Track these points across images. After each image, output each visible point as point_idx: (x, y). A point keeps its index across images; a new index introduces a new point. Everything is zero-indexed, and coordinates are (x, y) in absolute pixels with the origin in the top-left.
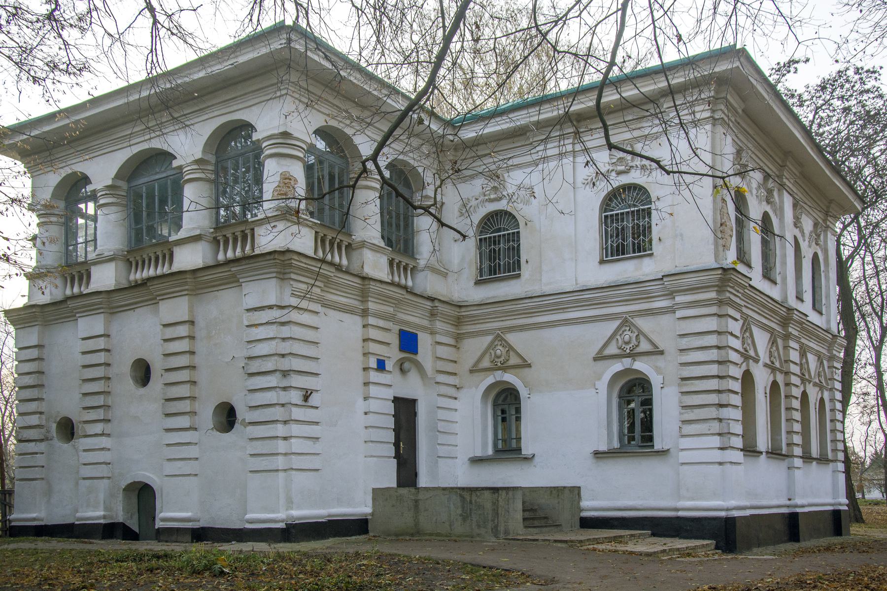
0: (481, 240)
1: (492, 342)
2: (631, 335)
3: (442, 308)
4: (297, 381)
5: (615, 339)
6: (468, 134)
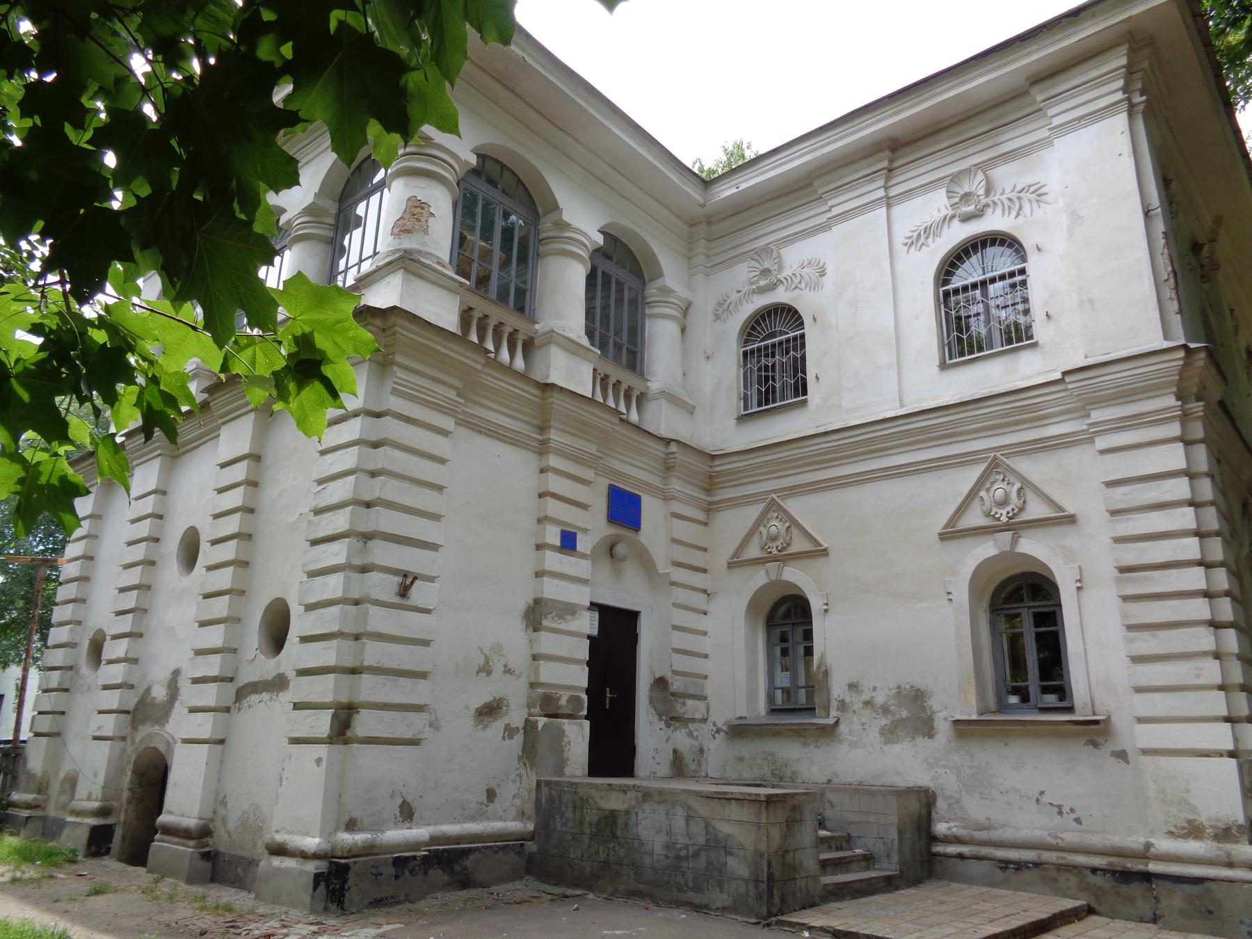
0: (745, 354)
3: (681, 456)
4: (383, 553)
5: (977, 499)
6: (726, 191)
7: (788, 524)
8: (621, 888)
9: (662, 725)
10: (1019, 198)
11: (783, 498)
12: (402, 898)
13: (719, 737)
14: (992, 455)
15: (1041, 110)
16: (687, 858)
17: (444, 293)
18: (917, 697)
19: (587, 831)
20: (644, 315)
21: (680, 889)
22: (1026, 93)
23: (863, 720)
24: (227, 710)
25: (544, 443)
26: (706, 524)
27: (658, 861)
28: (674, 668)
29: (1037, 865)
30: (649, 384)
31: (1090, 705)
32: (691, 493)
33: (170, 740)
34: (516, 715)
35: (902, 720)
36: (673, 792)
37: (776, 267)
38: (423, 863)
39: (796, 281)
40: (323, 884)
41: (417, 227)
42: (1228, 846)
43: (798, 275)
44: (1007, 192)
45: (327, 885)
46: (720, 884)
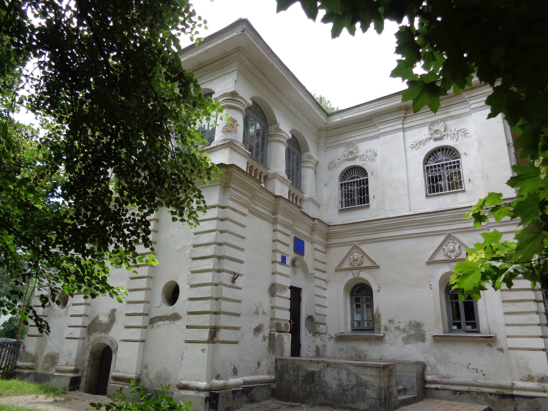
0: (341, 185)
1: (351, 250)
2: (455, 246)
3: (319, 226)
4: (228, 265)
7: (362, 255)
8: (317, 402)
9: (311, 335)
10: (457, 134)
12: (235, 407)
13: (332, 340)
14: (448, 232)
15: (466, 101)
16: (348, 390)
17: (242, 157)
18: (418, 326)
19: (301, 379)
20: (301, 166)
21: (345, 402)
23: (395, 335)
24: (146, 327)
25: (276, 219)
26: (325, 253)
27: (335, 391)
28: (316, 312)
29: (468, 392)
30: (304, 195)
31: (488, 331)
32: (323, 241)
33: (113, 340)
34: (266, 332)
35: (411, 335)
36: (340, 364)
37: (356, 151)
38: (242, 393)
39: (365, 157)
40: (208, 401)
41: (233, 130)
42: (543, 384)
44: (452, 131)
45: (210, 402)
46: (363, 401)
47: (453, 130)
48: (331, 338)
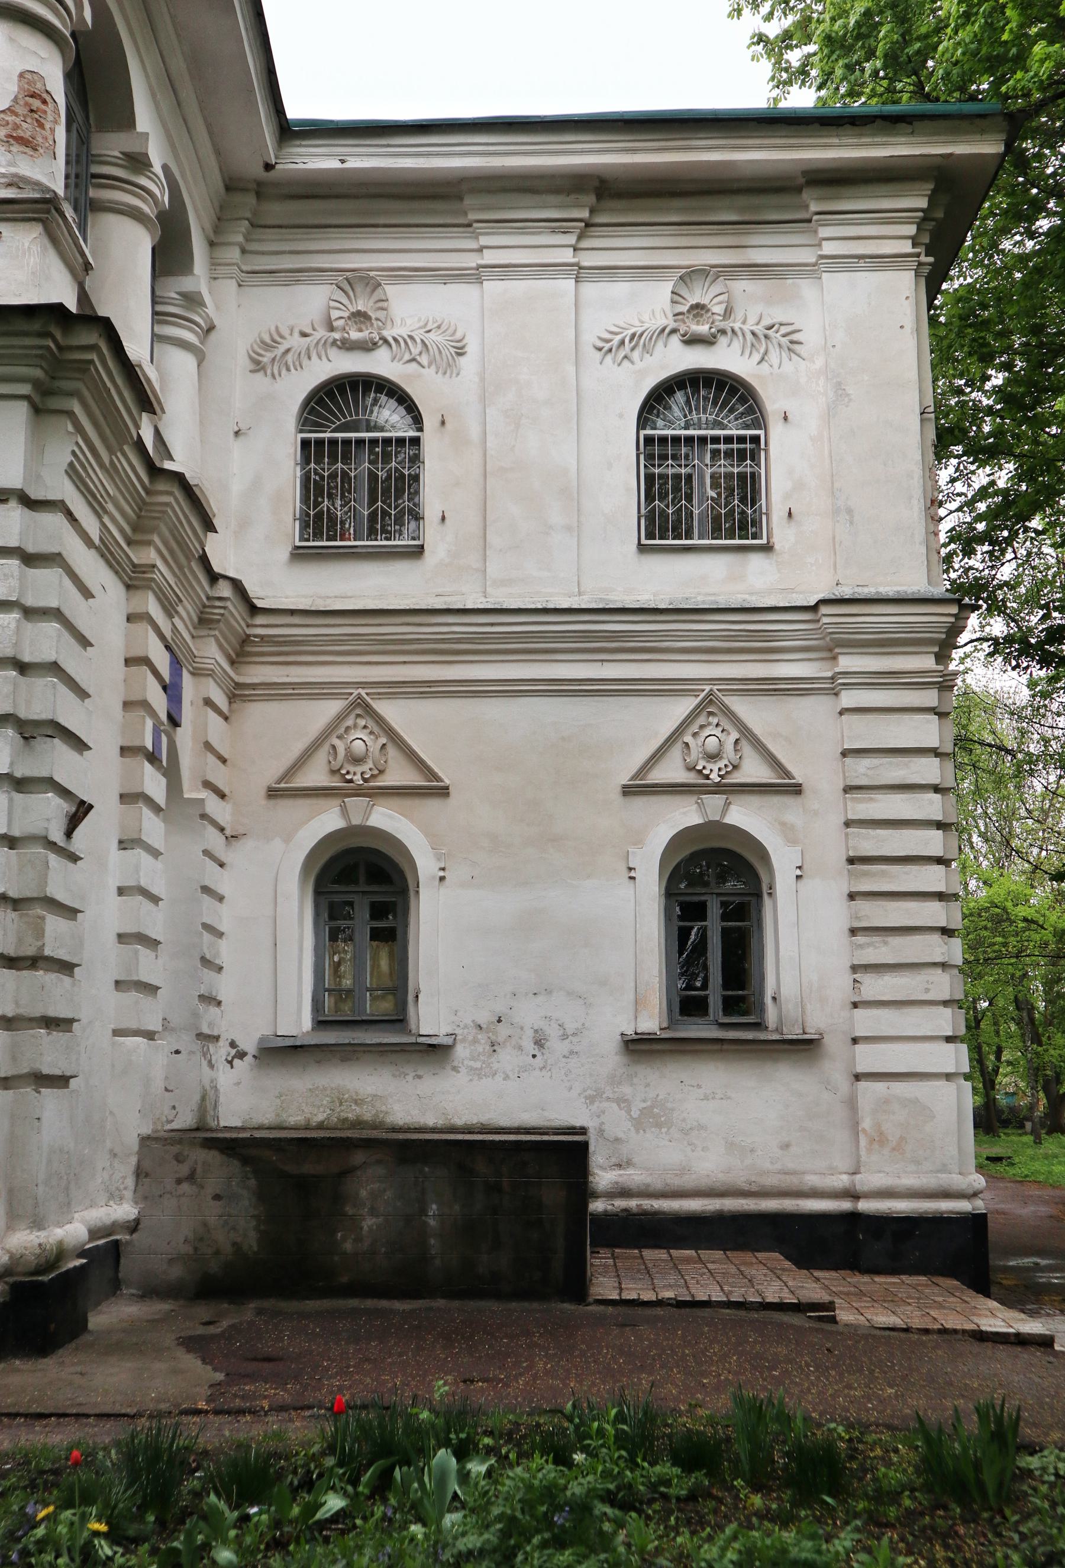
1: (340, 718)
10: (766, 337)
11: (380, 696)
14: (707, 688)
15: (809, 221)
22: (799, 190)
26: (226, 719)
43: (418, 341)
47: (752, 320)
48: (241, 1055)
